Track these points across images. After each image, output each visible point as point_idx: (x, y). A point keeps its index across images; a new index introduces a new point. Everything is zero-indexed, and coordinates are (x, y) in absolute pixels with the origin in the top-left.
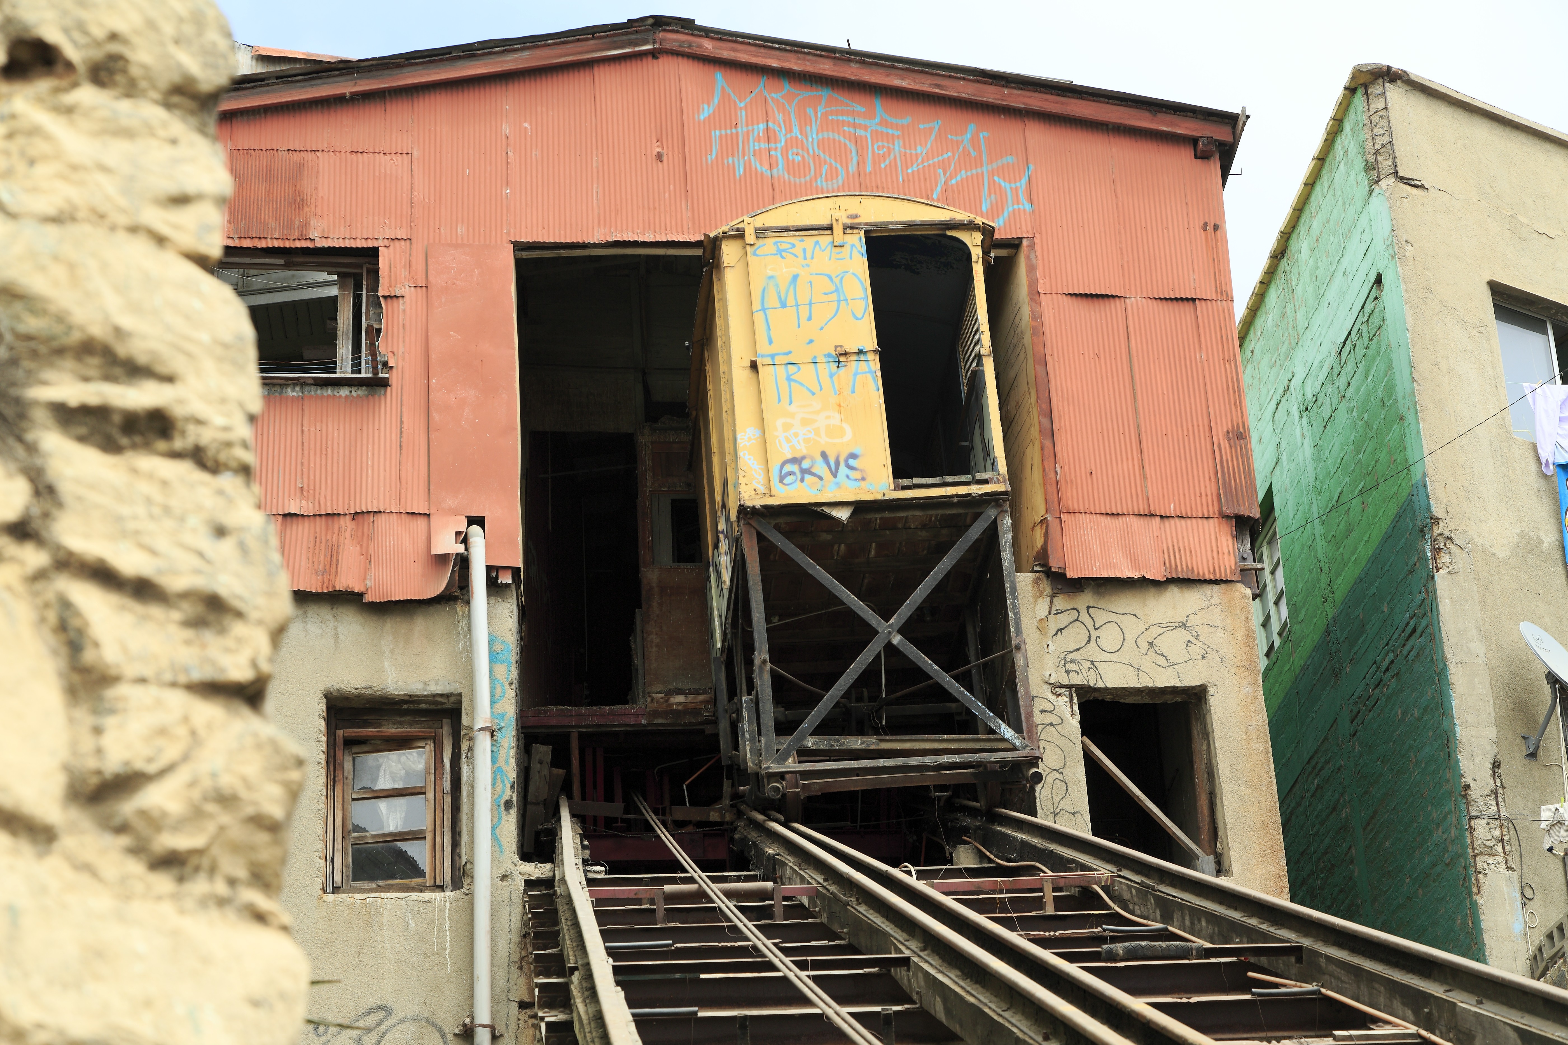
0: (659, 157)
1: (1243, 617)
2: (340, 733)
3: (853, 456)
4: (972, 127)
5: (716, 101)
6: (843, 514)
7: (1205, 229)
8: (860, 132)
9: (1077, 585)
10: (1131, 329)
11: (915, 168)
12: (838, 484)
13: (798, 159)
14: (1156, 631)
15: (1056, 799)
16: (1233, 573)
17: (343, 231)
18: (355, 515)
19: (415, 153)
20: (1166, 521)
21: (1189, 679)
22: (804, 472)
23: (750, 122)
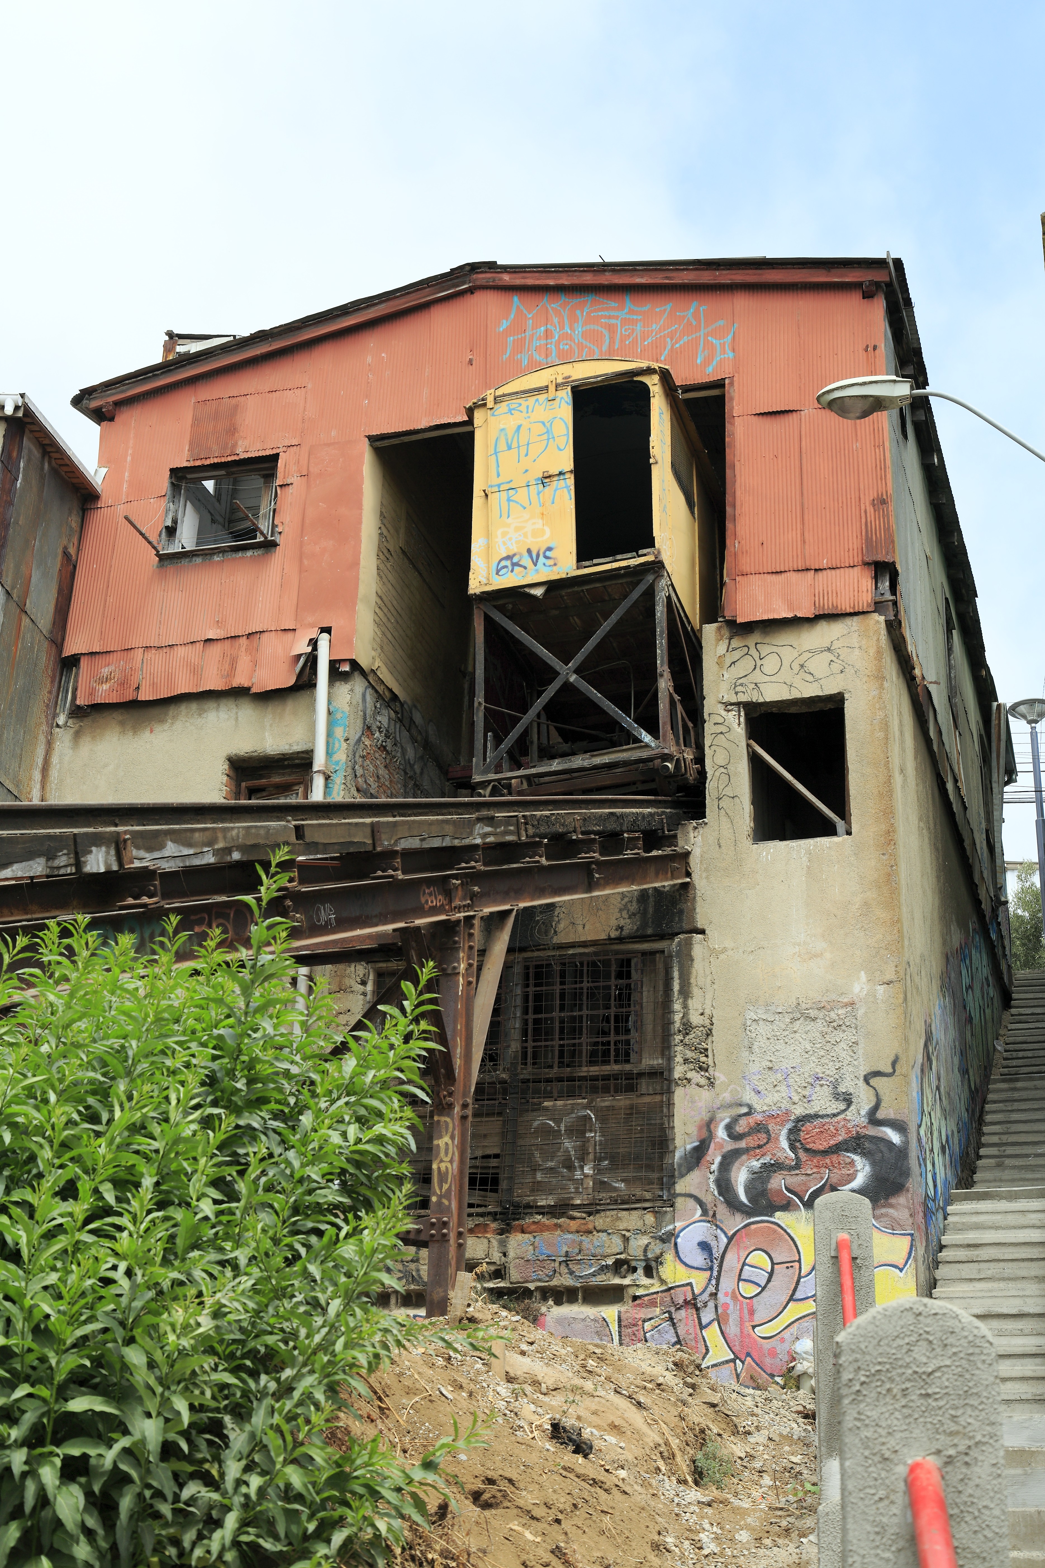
0: (471, 362)
1: (875, 638)
2: (243, 784)
3: (550, 549)
4: (695, 304)
5: (512, 316)
6: (538, 592)
7: (866, 350)
8: (613, 321)
9: (749, 628)
10: (803, 433)
11: (650, 340)
12: (537, 571)
13: (567, 347)
14: (807, 655)
15: (721, 788)
16: (869, 605)
17: (259, 446)
18: (249, 635)
19: (310, 386)
20: (820, 574)
21: (830, 688)
22: (514, 565)
23: (535, 327)
